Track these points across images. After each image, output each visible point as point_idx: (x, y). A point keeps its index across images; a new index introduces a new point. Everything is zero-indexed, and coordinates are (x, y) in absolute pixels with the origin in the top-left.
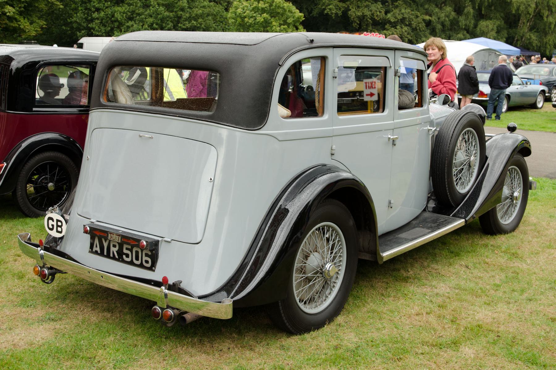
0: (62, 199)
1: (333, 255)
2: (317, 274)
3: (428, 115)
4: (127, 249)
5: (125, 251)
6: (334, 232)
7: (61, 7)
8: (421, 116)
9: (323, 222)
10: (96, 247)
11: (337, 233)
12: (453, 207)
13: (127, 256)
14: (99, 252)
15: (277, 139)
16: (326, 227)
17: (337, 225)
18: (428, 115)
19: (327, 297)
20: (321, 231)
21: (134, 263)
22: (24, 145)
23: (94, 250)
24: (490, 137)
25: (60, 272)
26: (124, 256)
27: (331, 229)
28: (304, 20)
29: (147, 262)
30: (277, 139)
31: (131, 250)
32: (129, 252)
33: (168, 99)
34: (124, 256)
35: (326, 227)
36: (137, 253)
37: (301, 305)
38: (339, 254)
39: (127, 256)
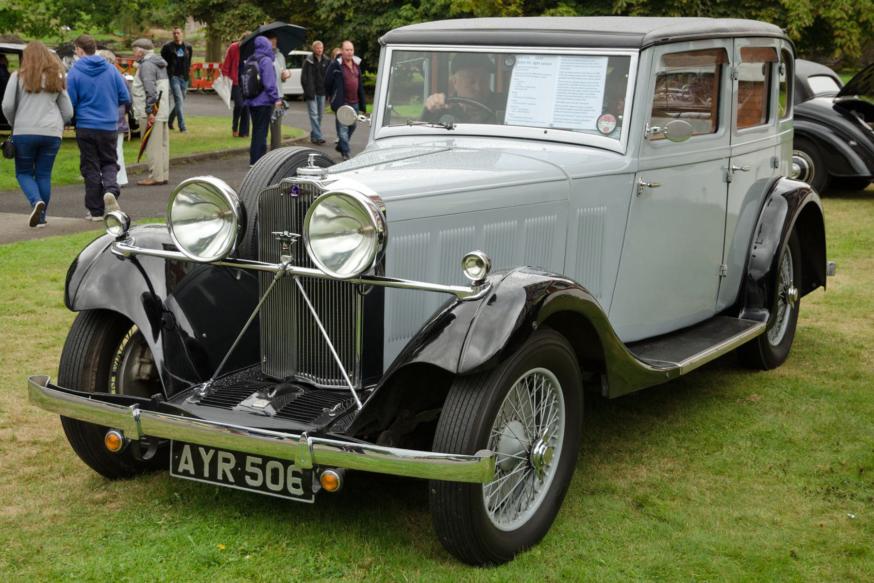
1: (535, 390)
6: (550, 386)
7: (94, 8)
9: (529, 370)
10: (186, 462)
11: (553, 389)
13: (254, 477)
14: (192, 472)
16: (535, 376)
19: (536, 492)
20: (526, 384)
21: (247, 484)
22: (188, 356)
23: (180, 470)
27: (544, 380)
28: (492, 63)
31: (263, 467)
32: (258, 471)
33: (508, 456)
35: (535, 376)
36: (275, 471)
37: (491, 514)
38: (553, 402)
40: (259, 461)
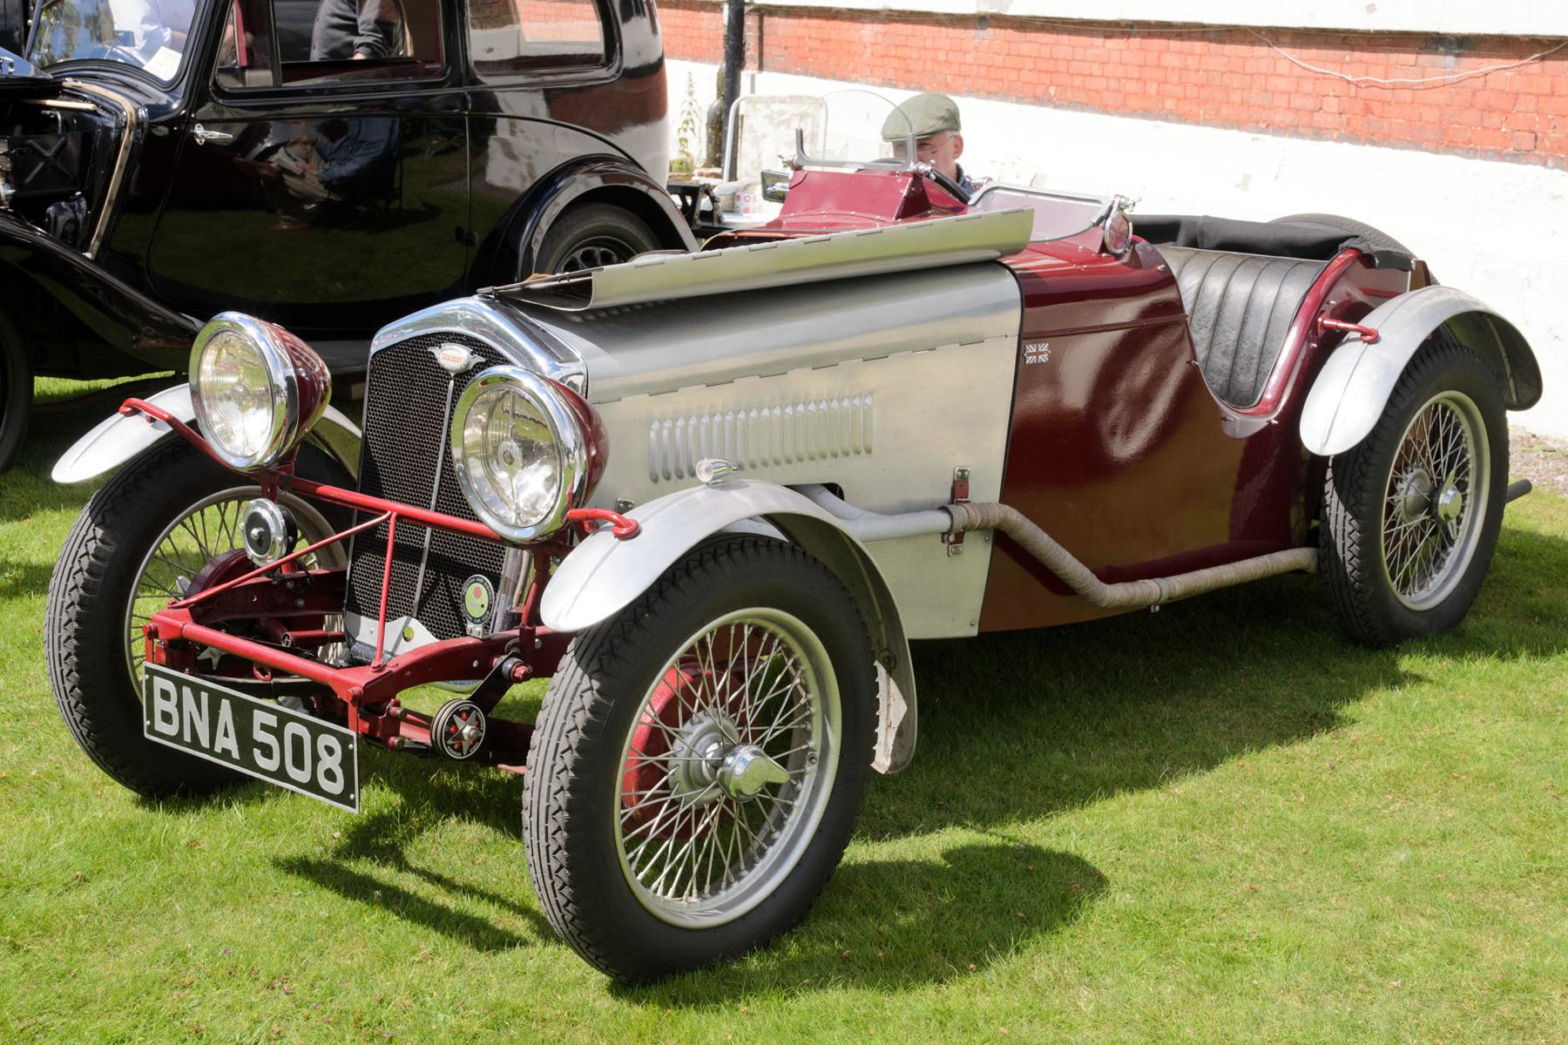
0: (182, 671)
2: (743, 681)
3: (433, 503)
4: (264, 727)
5: (260, 736)
8: (358, 524)
10: (226, 734)
12: (1027, 306)
13: (267, 751)
15: (1336, 415)
17: (1477, 405)
18: (433, 503)
24: (231, 533)
25: (303, 868)
26: (257, 752)
29: (330, 775)
30: (1336, 415)
32: (270, 739)
34: (257, 752)
39: (267, 751)
40: (272, 721)
